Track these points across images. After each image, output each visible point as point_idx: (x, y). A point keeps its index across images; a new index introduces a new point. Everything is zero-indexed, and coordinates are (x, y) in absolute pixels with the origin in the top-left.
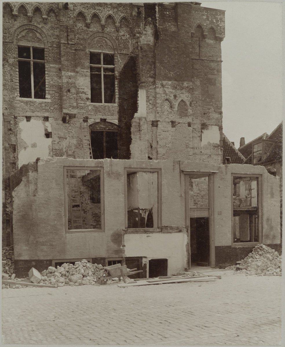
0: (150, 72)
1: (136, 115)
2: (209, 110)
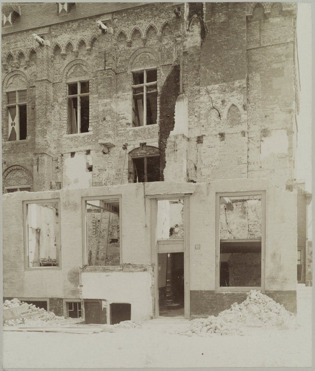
0: (196, 79)
1: (172, 133)
2: (273, 110)
